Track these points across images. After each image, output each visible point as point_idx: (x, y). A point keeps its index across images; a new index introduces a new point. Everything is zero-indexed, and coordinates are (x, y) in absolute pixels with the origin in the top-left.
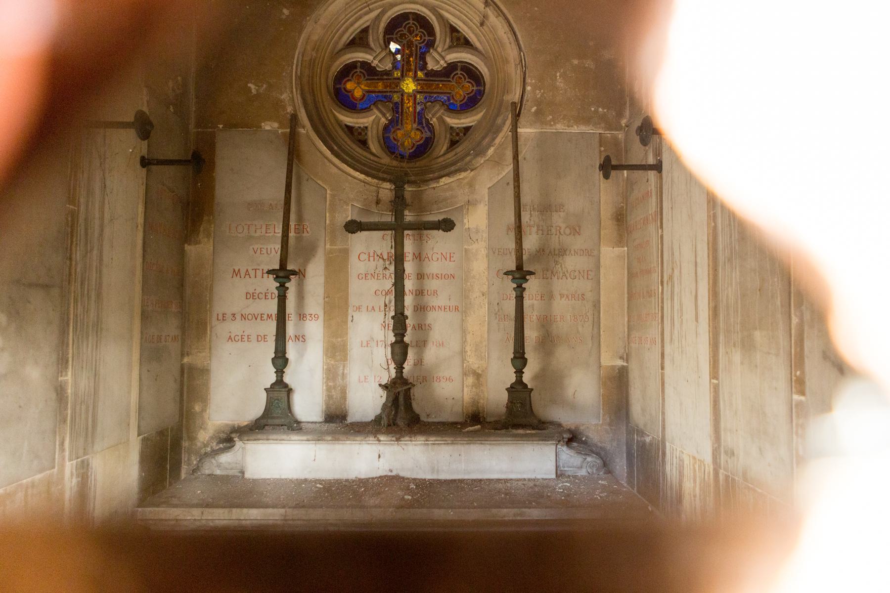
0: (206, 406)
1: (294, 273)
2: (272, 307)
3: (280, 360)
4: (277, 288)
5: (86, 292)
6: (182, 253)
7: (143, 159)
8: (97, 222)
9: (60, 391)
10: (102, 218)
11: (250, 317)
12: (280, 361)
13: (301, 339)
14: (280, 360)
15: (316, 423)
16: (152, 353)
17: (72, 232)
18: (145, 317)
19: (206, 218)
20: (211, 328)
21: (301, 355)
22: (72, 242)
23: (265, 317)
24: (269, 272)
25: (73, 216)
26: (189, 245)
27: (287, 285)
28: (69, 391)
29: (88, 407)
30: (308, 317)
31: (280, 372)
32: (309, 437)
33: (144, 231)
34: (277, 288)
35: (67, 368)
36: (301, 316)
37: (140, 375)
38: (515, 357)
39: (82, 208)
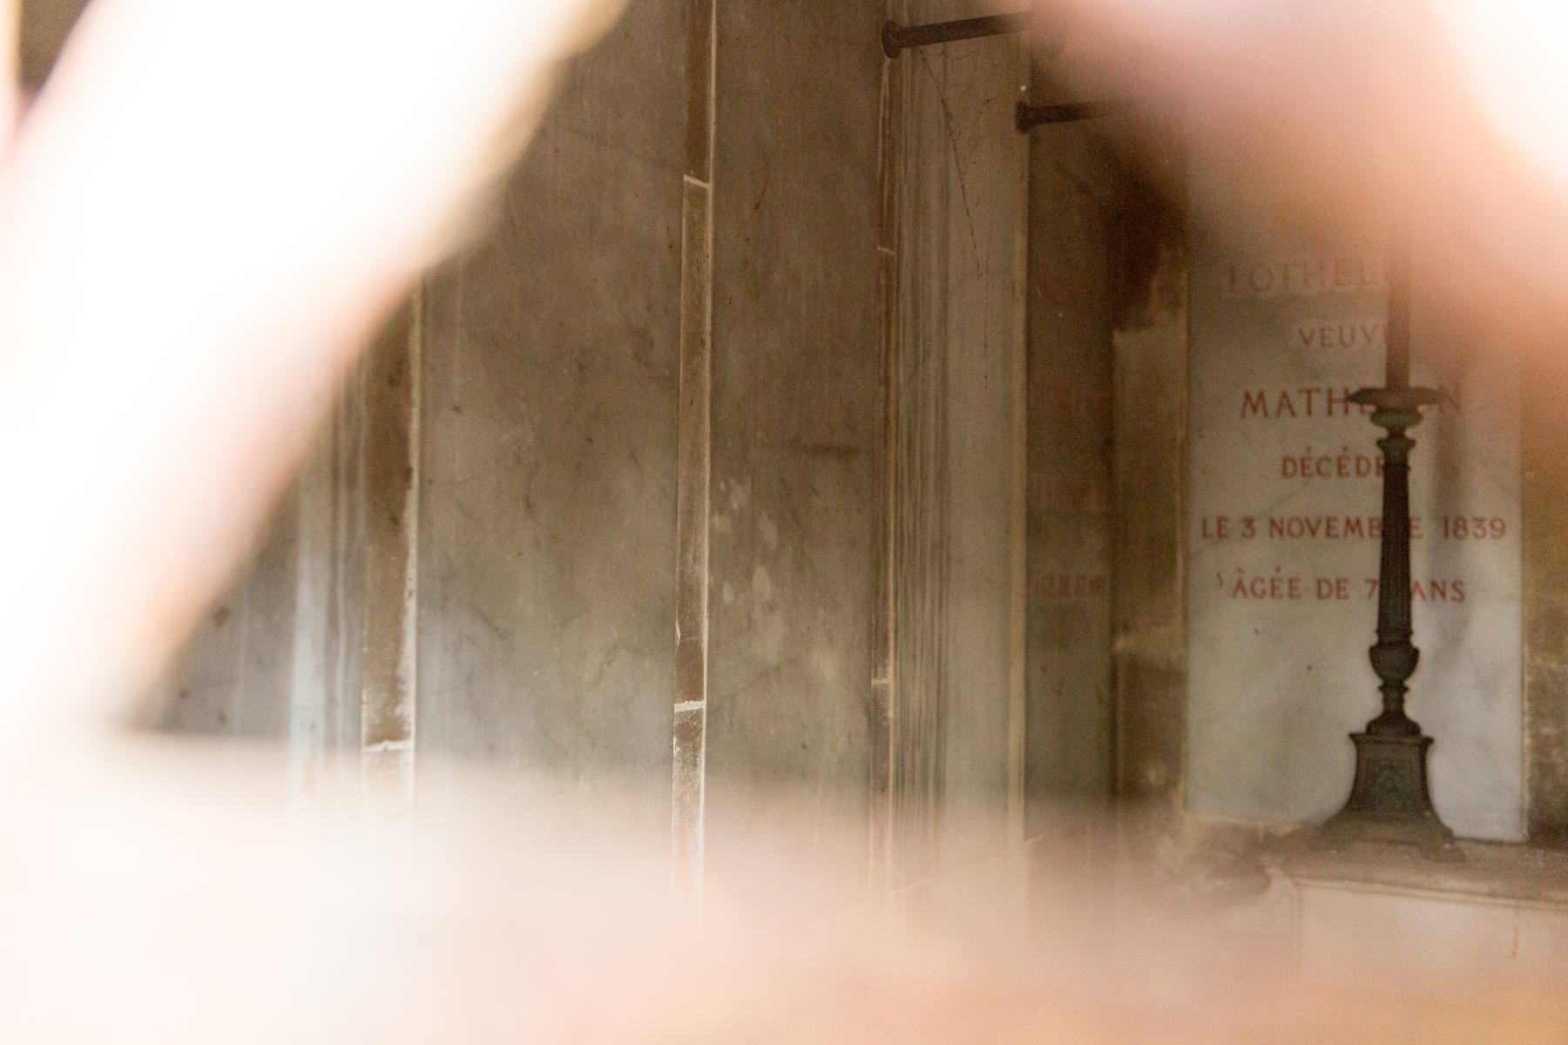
0: (1177, 771)
1: (1430, 396)
2: (1368, 499)
3: (1394, 655)
4: (1380, 443)
5: (918, 466)
6: (1108, 355)
7: (1022, 109)
8: (935, 285)
9: (873, 709)
10: (944, 276)
11: (1295, 527)
12: (1394, 658)
13: (1450, 592)
14: (1394, 655)
15: (1500, 843)
16: (1049, 627)
17: (888, 314)
18: (1034, 528)
19: (1165, 254)
20: (1187, 558)
21: (1453, 639)
22: (888, 339)
23: (1340, 527)
24: (1361, 397)
25: (889, 269)
26: (1123, 330)
27: (1410, 433)
28: (891, 714)
29: (925, 759)
30: (1471, 527)
31: (1393, 688)
32: (1496, 885)
33: (1028, 303)
34: (1380, 443)
35: (885, 655)
36: (1452, 526)
37: (1027, 678)
38: (1380, 644)
39: (906, 248)
